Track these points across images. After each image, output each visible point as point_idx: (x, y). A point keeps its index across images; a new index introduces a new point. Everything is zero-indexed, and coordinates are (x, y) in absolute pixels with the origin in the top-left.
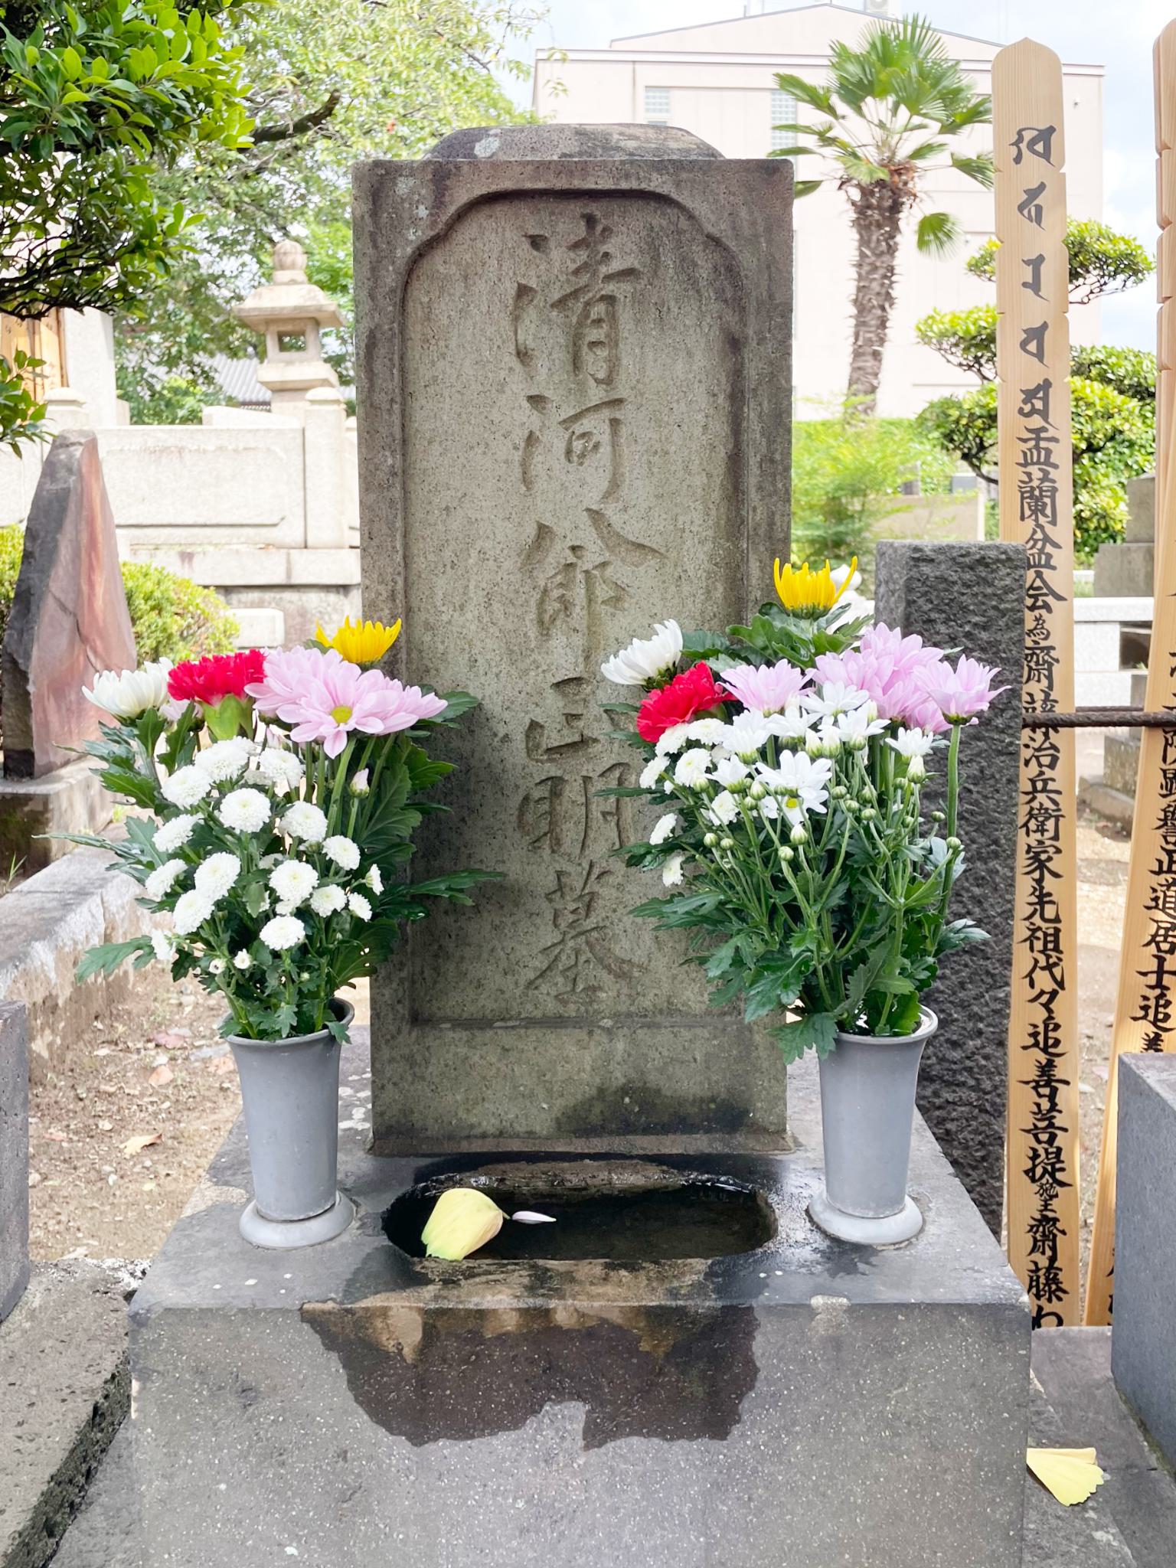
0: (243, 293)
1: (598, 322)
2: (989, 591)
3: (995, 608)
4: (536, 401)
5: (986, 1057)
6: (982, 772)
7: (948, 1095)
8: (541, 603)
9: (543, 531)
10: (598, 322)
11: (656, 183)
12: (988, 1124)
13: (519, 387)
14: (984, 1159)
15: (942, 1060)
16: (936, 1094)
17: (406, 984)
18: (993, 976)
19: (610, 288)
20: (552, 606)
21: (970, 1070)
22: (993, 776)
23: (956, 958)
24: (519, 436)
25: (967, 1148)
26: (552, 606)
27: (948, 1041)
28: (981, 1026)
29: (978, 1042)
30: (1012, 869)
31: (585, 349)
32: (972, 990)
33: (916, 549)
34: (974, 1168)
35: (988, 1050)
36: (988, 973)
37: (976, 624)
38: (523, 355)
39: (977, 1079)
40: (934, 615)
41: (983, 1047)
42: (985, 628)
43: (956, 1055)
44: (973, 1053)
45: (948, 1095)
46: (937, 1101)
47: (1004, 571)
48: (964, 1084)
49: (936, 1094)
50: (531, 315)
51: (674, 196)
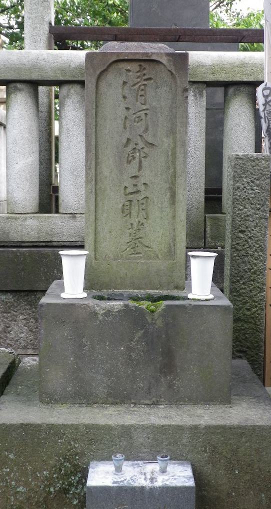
0: (126, 95)
1: (142, 90)
2: (259, 168)
3: (261, 174)
4: (127, 109)
5: (258, 314)
6: (257, 224)
7: (246, 326)
8: (128, 158)
9: (128, 140)
10: (142, 90)
11: (154, 58)
12: (259, 335)
13: (123, 106)
14: (257, 346)
15: (244, 315)
16: (242, 325)
17: (265, 412)
18: (260, 288)
19: (145, 83)
20: (130, 158)
21: (253, 318)
22: (260, 226)
23: (249, 283)
24: (123, 117)
25: (252, 343)
26: (130, 158)
27: (246, 309)
28: (256, 304)
29: (256, 309)
30: (266, 255)
31: (139, 97)
32: (254, 292)
33: (237, 155)
34: (254, 349)
35: (259, 312)
36: (259, 287)
37: (255, 179)
38: (124, 97)
39: (255, 321)
40: (242, 175)
41: (257, 311)
42: (257, 180)
43: (249, 313)
44: (254, 313)
45: (246, 326)
46: (243, 328)
47: (263, 162)
48: (251, 322)
49: (242, 325)
50: (125, 88)
51: (161, 61)
